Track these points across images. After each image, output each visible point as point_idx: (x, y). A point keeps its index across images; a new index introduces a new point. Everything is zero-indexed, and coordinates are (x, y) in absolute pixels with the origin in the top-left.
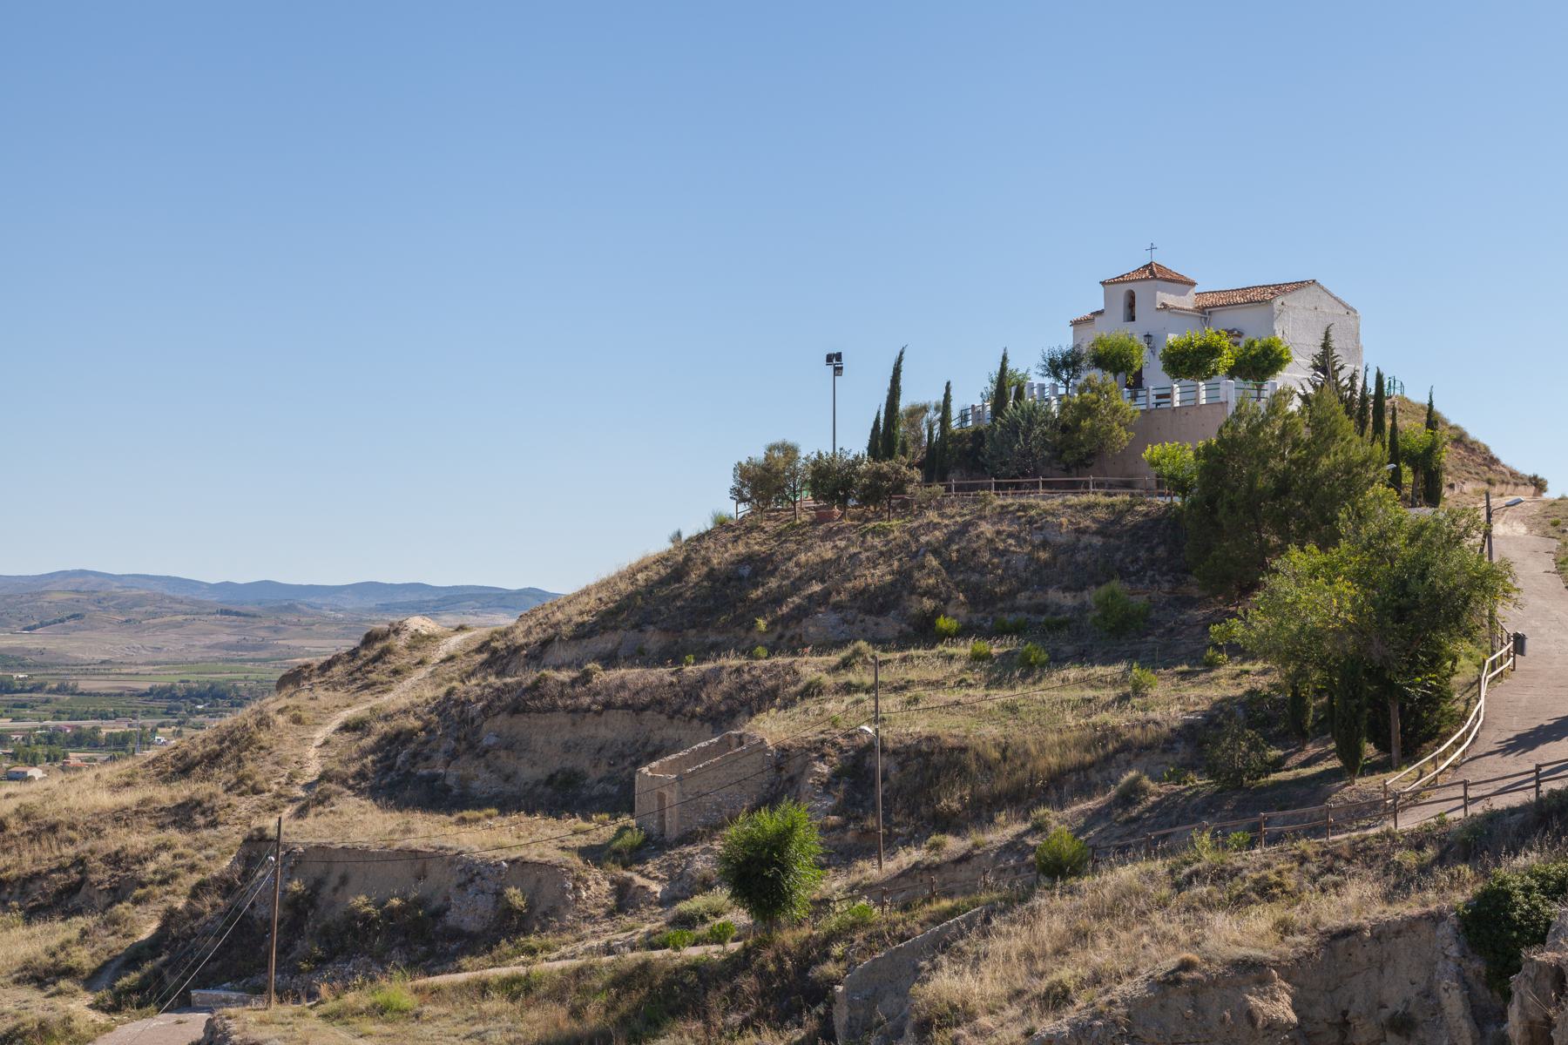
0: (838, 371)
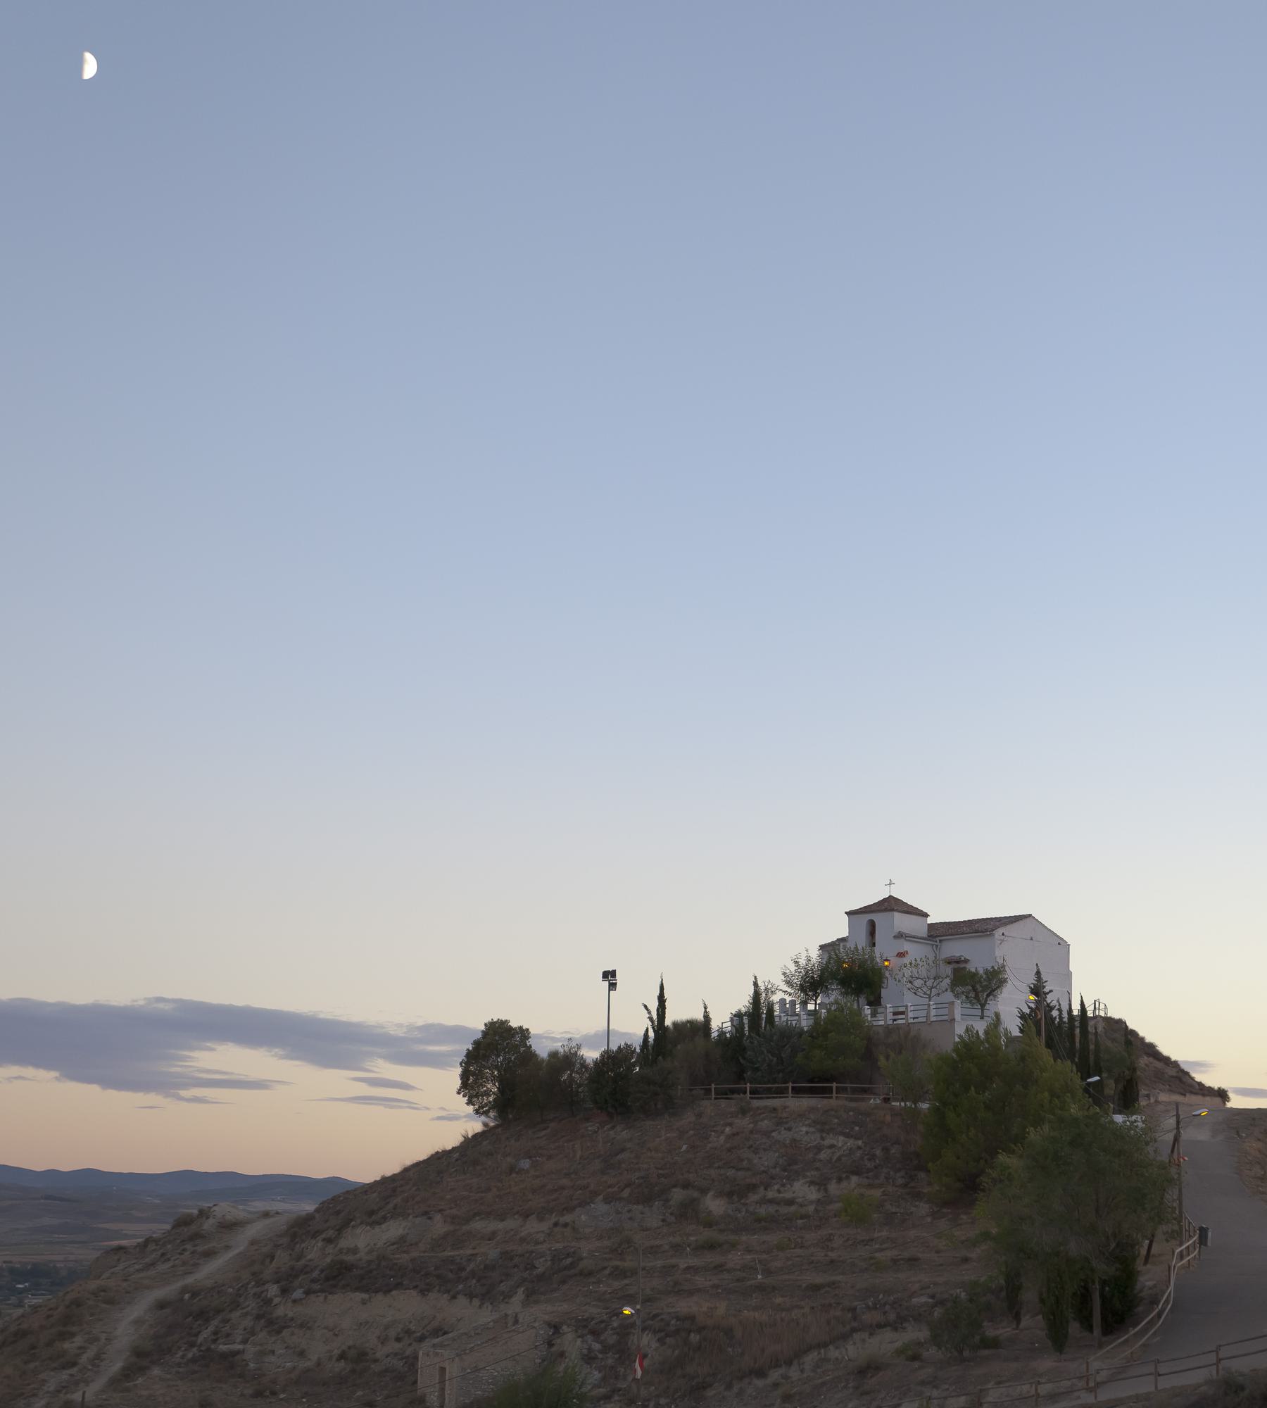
0: (613, 986)
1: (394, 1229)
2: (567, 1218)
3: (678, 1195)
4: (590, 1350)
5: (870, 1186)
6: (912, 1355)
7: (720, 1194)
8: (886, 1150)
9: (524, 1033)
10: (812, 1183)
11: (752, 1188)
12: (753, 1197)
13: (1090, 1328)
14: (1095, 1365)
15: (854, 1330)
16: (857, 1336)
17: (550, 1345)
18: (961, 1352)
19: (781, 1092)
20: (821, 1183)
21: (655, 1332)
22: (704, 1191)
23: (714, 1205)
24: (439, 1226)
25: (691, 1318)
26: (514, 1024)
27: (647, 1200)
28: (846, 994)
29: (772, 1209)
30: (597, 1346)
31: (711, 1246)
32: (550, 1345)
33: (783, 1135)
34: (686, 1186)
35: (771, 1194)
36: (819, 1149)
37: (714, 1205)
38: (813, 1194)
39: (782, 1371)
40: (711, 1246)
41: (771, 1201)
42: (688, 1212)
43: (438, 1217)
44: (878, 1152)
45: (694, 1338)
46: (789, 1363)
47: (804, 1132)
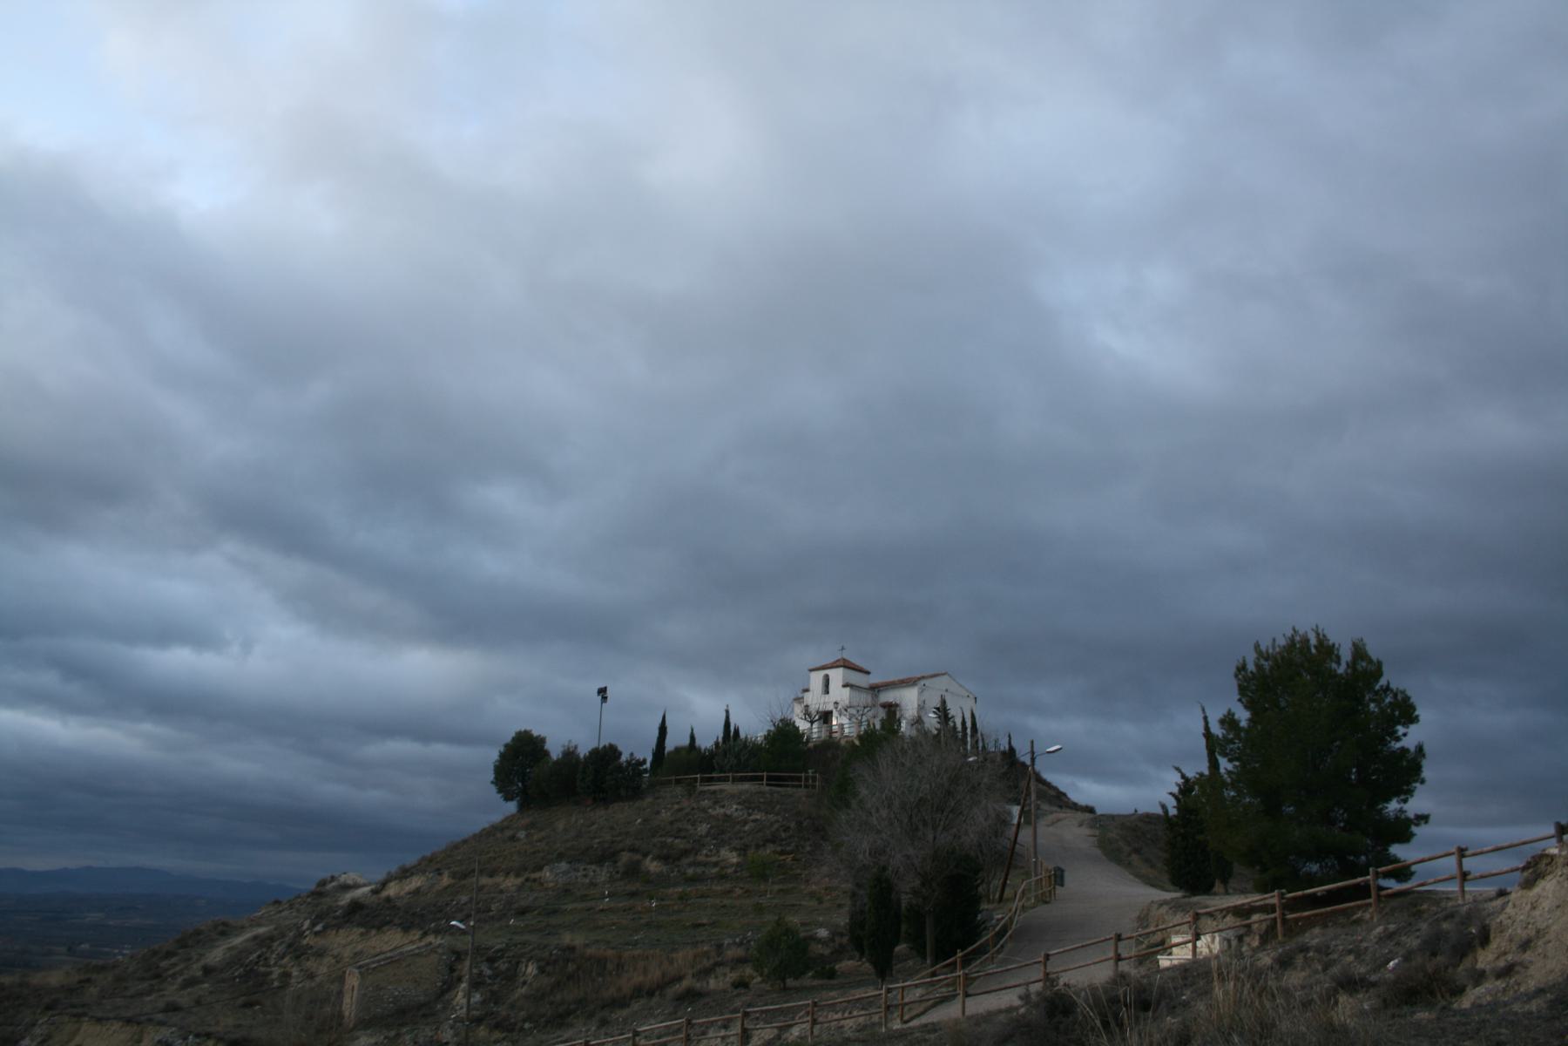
0: (604, 699)
1: (416, 882)
2: (537, 875)
3: (625, 857)
4: (480, 974)
5: (782, 853)
6: (742, 984)
7: (658, 858)
8: (799, 823)
9: (542, 740)
10: (735, 849)
11: (685, 853)
12: (685, 861)
13: (925, 958)
14: (560, 825)
15: (717, 964)
16: (719, 970)
17: (452, 970)
18: (783, 980)
19: (725, 780)
20: (743, 850)
21: (539, 961)
22: (645, 855)
23: (653, 866)
24: (446, 880)
25: (572, 949)
26: (535, 733)
27: (600, 861)
28: (1056, 994)
29: (699, 870)
30: (489, 972)
31: (633, 895)
32: (452, 970)
33: (719, 811)
34: (633, 850)
35: (701, 858)
36: (745, 823)
37: (653, 866)
38: (734, 858)
39: (643, 1001)
40: (633, 895)
41: (699, 864)
42: (633, 871)
43: (446, 874)
44: (793, 825)
45: (571, 967)
46: (651, 994)
47: (733, 809)
